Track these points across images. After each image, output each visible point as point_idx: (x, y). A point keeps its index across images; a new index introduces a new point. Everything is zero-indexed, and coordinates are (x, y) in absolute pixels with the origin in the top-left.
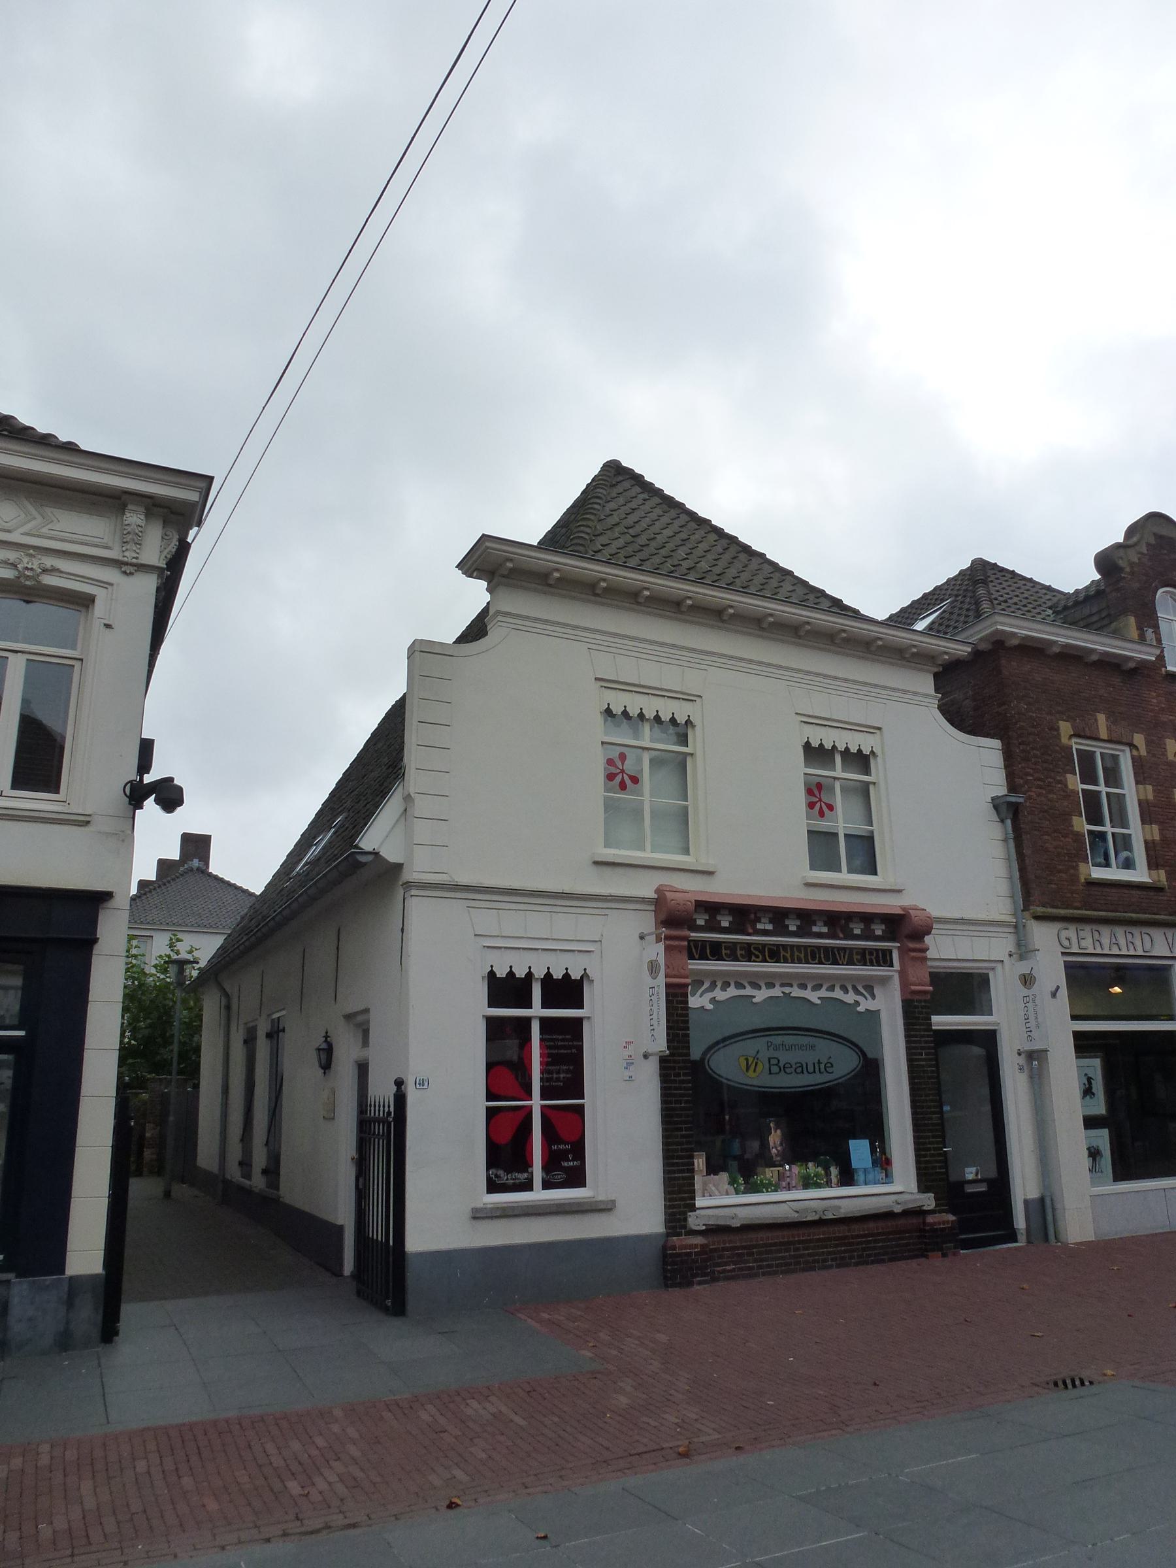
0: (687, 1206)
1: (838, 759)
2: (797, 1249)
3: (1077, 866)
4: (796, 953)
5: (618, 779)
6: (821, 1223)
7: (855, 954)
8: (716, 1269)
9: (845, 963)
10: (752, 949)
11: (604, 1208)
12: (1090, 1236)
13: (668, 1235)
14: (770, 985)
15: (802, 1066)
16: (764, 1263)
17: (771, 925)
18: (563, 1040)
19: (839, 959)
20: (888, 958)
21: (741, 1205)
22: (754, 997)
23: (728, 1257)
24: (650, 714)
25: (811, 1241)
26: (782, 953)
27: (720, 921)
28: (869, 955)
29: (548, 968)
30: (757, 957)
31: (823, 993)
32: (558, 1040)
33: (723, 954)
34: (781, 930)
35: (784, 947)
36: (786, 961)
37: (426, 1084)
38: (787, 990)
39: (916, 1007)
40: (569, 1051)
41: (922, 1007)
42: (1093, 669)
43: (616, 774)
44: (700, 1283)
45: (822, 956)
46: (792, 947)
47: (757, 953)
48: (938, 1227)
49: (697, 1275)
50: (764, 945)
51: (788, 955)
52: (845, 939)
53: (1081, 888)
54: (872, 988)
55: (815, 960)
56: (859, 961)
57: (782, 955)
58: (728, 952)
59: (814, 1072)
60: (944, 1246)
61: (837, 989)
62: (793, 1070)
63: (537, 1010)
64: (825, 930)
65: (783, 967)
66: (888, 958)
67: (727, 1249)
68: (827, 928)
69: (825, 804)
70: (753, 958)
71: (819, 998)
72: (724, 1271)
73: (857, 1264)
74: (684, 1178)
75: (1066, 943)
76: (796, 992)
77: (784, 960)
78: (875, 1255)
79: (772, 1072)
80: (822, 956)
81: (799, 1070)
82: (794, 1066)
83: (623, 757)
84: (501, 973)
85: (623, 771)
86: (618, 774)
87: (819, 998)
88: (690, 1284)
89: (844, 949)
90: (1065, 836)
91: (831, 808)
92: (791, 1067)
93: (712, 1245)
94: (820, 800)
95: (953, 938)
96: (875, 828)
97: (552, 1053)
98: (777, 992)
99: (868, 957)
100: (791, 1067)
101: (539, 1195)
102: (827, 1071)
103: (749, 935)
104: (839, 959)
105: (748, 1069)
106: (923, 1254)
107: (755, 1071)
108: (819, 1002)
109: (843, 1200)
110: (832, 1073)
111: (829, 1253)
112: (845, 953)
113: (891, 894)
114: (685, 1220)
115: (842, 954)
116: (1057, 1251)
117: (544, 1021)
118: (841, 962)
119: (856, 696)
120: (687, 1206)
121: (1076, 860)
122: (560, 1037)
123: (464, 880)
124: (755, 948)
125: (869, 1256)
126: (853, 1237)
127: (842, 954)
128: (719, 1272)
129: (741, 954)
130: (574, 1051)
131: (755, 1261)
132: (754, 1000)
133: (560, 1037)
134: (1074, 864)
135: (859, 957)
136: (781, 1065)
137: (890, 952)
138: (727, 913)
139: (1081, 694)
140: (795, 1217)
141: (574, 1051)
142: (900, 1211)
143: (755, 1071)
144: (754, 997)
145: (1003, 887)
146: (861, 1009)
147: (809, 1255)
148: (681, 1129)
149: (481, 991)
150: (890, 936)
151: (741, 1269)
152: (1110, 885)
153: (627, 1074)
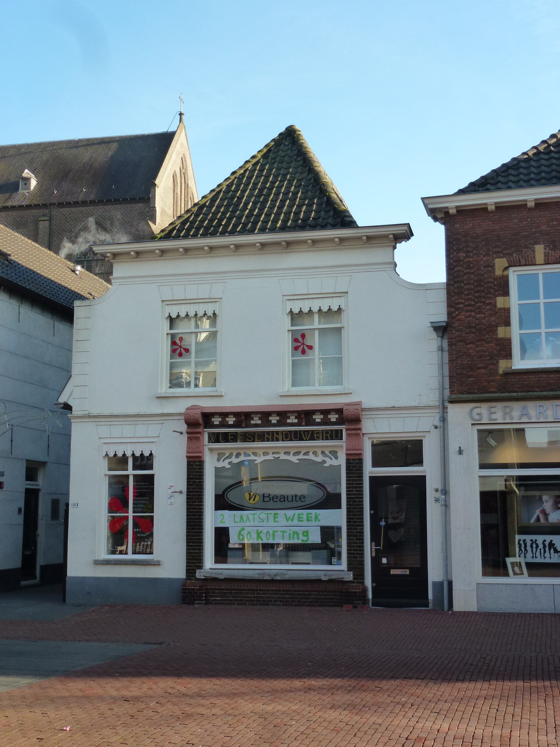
0: (196, 566)
1: (316, 317)
2: (260, 594)
3: (498, 362)
4: (276, 435)
5: (301, 348)
6: (273, 581)
7: (230, 436)
8: (211, 598)
9: (308, 439)
10: (247, 436)
11: (157, 564)
12: (473, 607)
13: (187, 579)
14: (265, 454)
15: (284, 498)
16: (313, 597)
17: (297, 420)
18: (144, 485)
19: (304, 437)
20: (339, 435)
21: (237, 569)
22: (256, 460)
23: (218, 593)
24: (315, 309)
25: (268, 590)
26: (266, 436)
27: (271, 420)
28: (325, 434)
29: (133, 451)
30: (250, 439)
31: (301, 456)
32: (142, 485)
33: (229, 439)
34: (267, 423)
35: (268, 433)
36: (268, 440)
37: (76, 505)
38: (277, 456)
39: (352, 463)
40: (147, 490)
41: (356, 463)
42: (538, 211)
43: (177, 349)
44: (198, 604)
45: (293, 436)
46: (273, 432)
47: (250, 437)
48: (352, 591)
49: (197, 600)
50: (254, 433)
51: (270, 437)
52: (306, 425)
53: (498, 377)
54: (336, 452)
55: (288, 438)
56: (232, 439)
57: (266, 437)
58: (232, 437)
59: (292, 501)
60: (355, 602)
61: (311, 453)
62: (278, 499)
63: (130, 471)
64: (296, 421)
65: (271, 444)
66: (339, 435)
67: (217, 589)
68: (297, 420)
69: (183, 348)
70: (248, 440)
71: (298, 460)
72: (215, 600)
73: (295, 605)
74: (195, 553)
75: (477, 417)
76: (283, 457)
77: (276, 439)
78: (310, 602)
79: (265, 501)
80: (293, 436)
81: (282, 500)
82: (279, 498)
83: (303, 336)
84: (138, 454)
85: (181, 347)
86: (178, 349)
87: (298, 460)
88: (193, 604)
89: (308, 431)
90: (490, 342)
91: (311, 348)
92: (277, 498)
93: (282, 588)
94: (303, 344)
95: (389, 420)
96: (169, 360)
97: (138, 492)
98: (270, 457)
99: (324, 435)
100: (277, 498)
101: (130, 556)
102: (301, 501)
103: (243, 428)
104: (304, 437)
105: (250, 499)
106: (340, 604)
107: (254, 500)
108: (298, 462)
109: (246, 571)
110: (305, 501)
111: (278, 598)
112: (308, 434)
113: (199, 398)
114: (195, 573)
115: (306, 434)
116: (269, 614)
117: (135, 476)
118: (305, 439)
119: (344, 275)
120: (196, 566)
121: (497, 358)
122: (143, 484)
123: (94, 412)
124: (249, 435)
125: (306, 602)
126: (295, 591)
127: (306, 434)
128: (212, 600)
129: (316, 437)
130: (149, 490)
131: (233, 597)
132: (256, 462)
133: (143, 484)
134: (495, 361)
135: (242, 437)
136: (271, 497)
137: (341, 431)
138: (320, 414)
139: (521, 234)
140: (257, 577)
141: (149, 490)
142: (327, 580)
143: (254, 500)
144: (256, 460)
145: (435, 383)
146: (326, 465)
147: (266, 597)
148: (194, 529)
149: (105, 464)
150: (340, 422)
151: (224, 600)
152: (552, 372)
153: (170, 501)
